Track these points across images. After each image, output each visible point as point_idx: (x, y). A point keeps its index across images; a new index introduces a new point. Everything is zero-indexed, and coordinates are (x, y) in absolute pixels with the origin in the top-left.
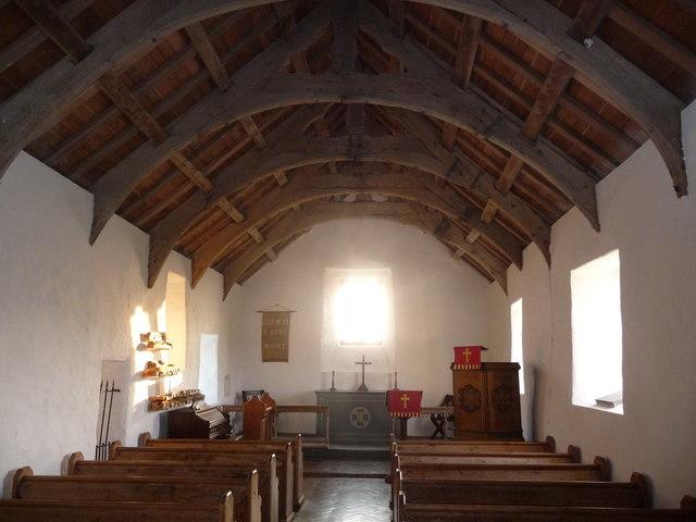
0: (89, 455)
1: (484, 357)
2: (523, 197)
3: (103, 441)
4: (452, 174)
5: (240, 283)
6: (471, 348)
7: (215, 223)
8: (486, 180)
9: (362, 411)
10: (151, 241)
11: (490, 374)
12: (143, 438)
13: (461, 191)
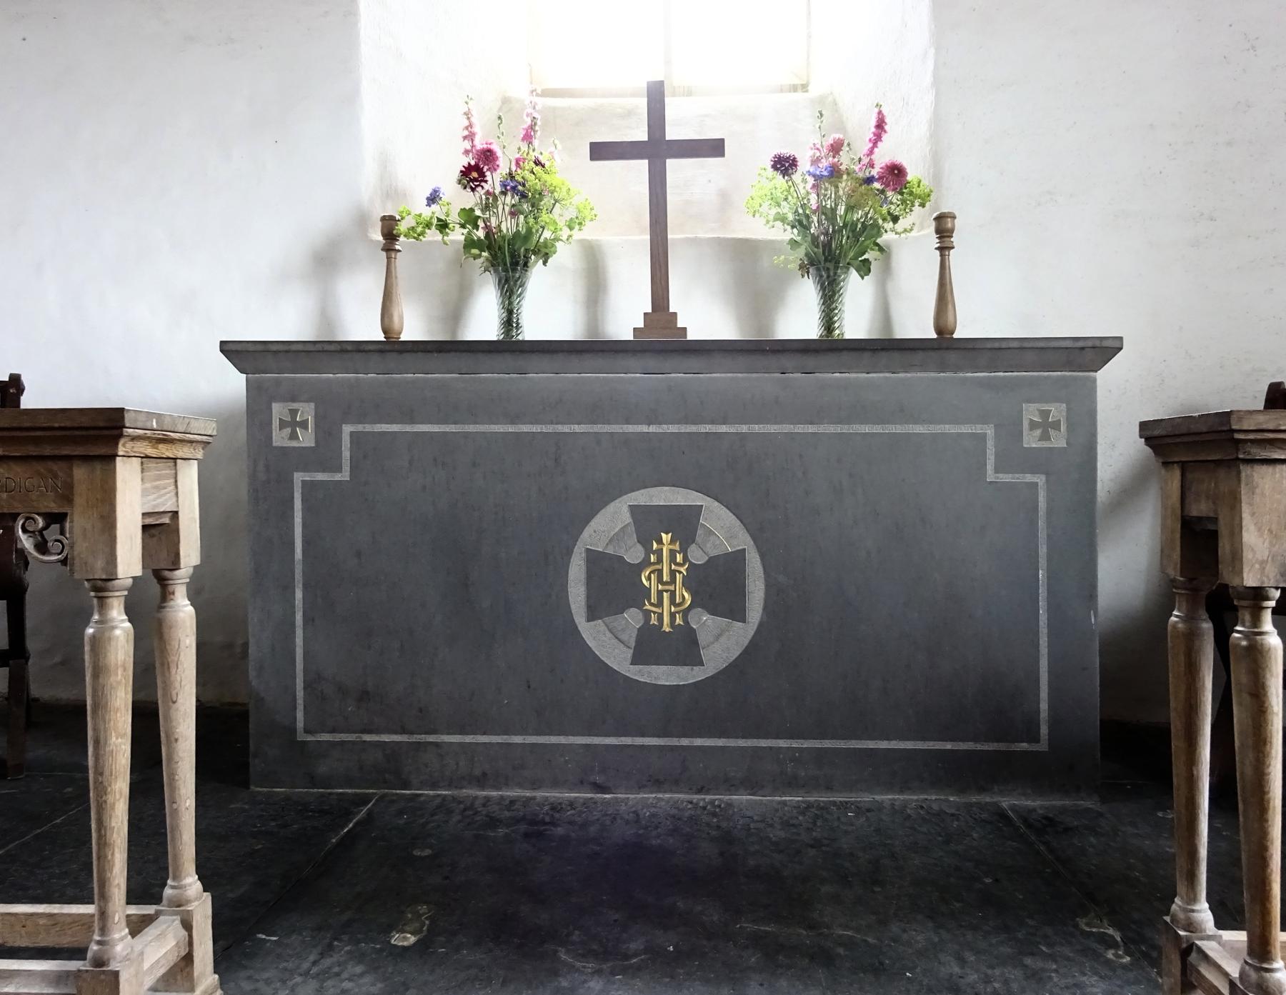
9: (684, 524)
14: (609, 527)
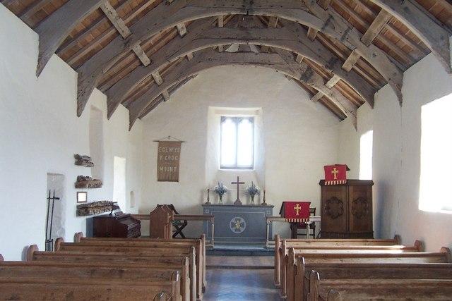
0: (42, 248)
1: (349, 175)
2: (384, 49)
3: (48, 238)
4: (327, 28)
5: (140, 118)
6: (337, 166)
7: (128, 65)
8: (354, 34)
10: (79, 77)
11: (351, 188)
12: (77, 235)
13: (328, 44)
14: (233, 220)
